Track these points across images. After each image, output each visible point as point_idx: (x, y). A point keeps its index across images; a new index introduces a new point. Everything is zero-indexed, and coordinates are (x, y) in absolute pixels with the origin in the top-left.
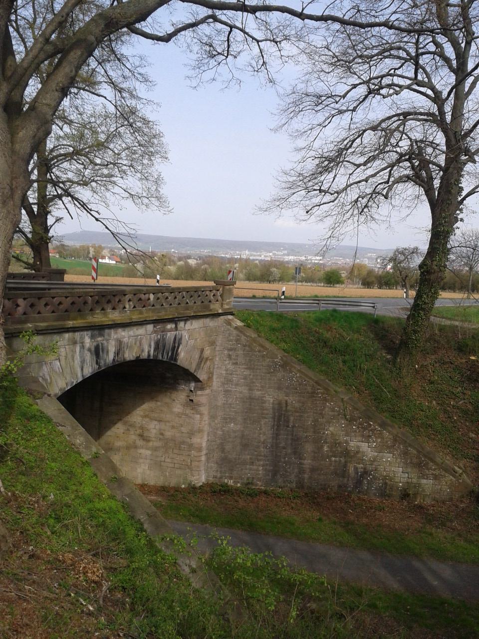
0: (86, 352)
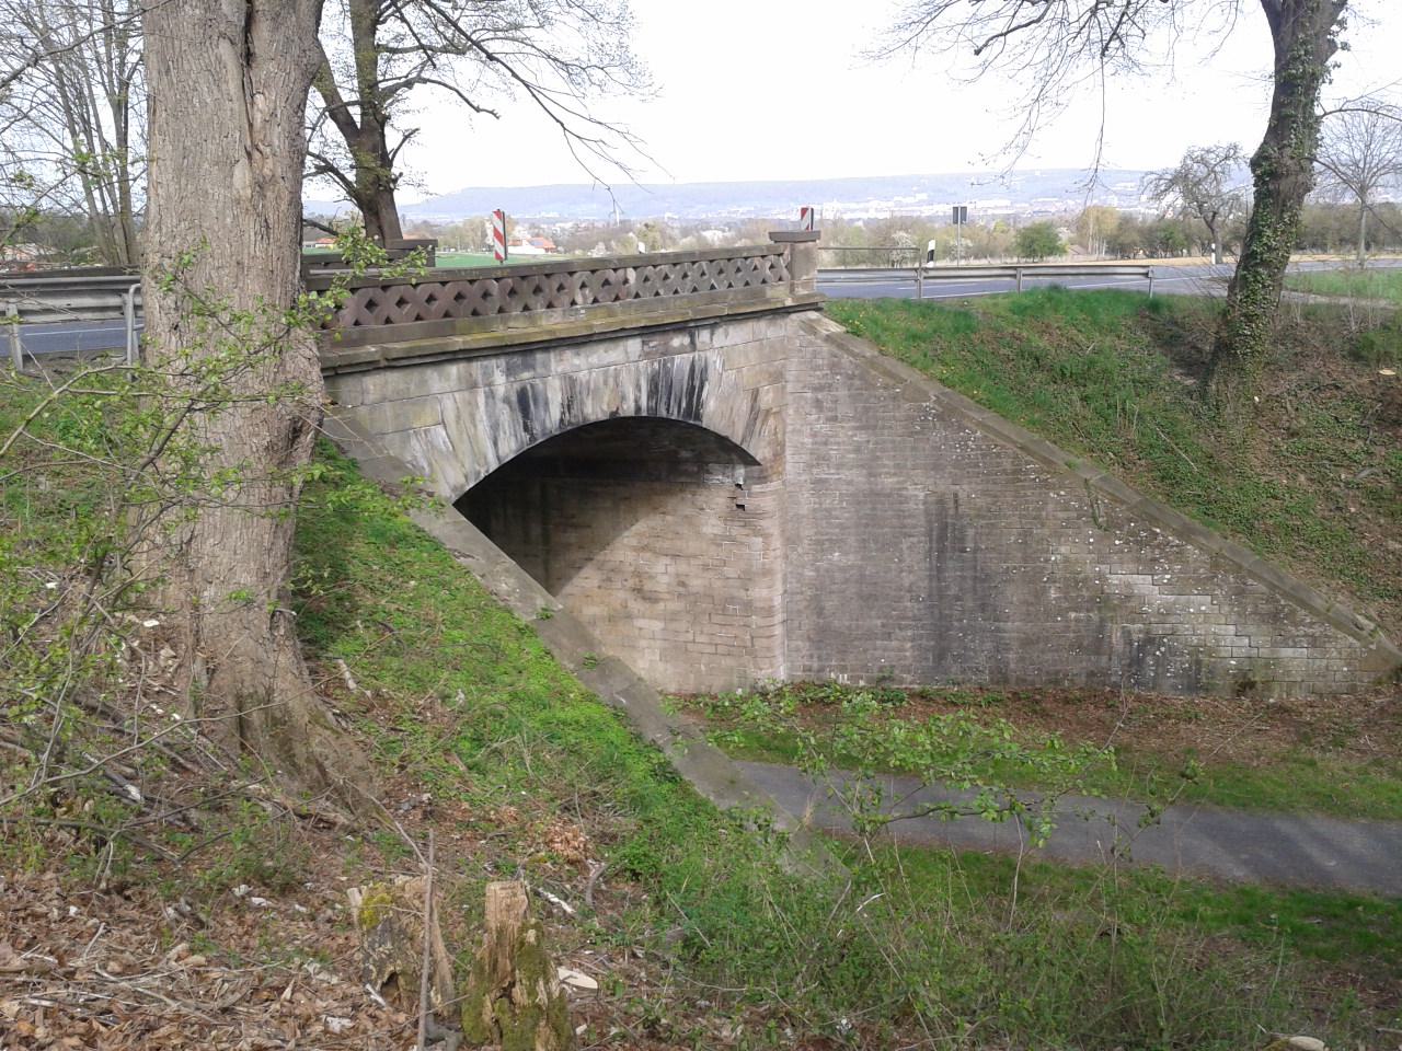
0: (500, 405)
